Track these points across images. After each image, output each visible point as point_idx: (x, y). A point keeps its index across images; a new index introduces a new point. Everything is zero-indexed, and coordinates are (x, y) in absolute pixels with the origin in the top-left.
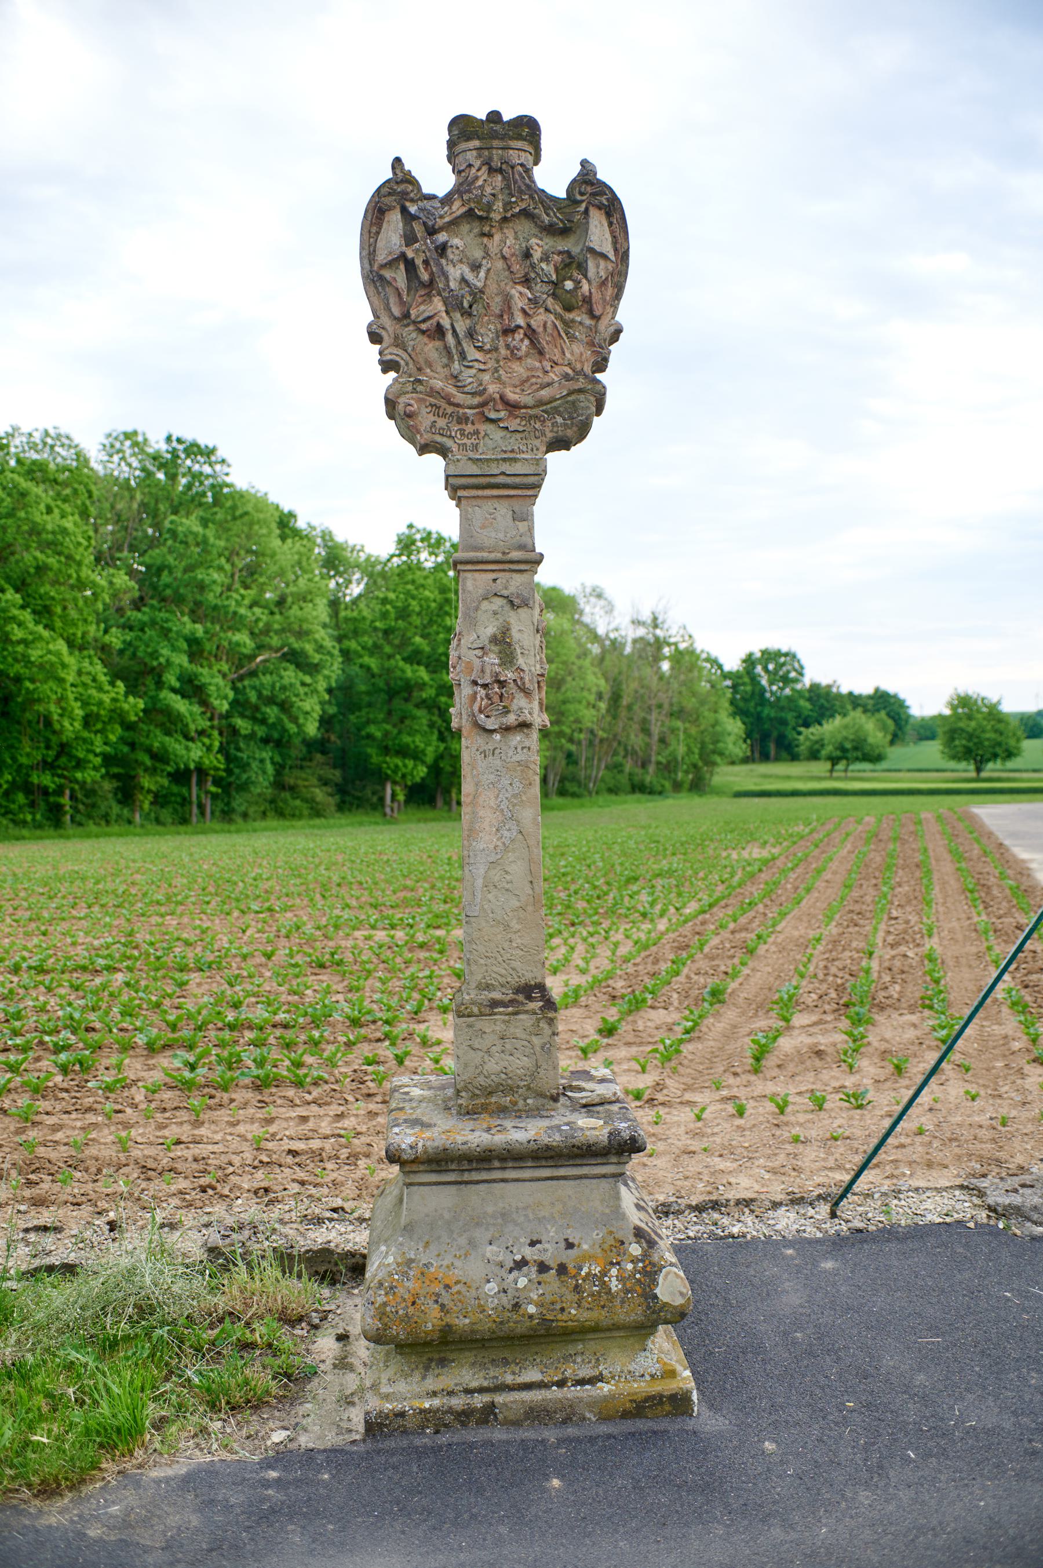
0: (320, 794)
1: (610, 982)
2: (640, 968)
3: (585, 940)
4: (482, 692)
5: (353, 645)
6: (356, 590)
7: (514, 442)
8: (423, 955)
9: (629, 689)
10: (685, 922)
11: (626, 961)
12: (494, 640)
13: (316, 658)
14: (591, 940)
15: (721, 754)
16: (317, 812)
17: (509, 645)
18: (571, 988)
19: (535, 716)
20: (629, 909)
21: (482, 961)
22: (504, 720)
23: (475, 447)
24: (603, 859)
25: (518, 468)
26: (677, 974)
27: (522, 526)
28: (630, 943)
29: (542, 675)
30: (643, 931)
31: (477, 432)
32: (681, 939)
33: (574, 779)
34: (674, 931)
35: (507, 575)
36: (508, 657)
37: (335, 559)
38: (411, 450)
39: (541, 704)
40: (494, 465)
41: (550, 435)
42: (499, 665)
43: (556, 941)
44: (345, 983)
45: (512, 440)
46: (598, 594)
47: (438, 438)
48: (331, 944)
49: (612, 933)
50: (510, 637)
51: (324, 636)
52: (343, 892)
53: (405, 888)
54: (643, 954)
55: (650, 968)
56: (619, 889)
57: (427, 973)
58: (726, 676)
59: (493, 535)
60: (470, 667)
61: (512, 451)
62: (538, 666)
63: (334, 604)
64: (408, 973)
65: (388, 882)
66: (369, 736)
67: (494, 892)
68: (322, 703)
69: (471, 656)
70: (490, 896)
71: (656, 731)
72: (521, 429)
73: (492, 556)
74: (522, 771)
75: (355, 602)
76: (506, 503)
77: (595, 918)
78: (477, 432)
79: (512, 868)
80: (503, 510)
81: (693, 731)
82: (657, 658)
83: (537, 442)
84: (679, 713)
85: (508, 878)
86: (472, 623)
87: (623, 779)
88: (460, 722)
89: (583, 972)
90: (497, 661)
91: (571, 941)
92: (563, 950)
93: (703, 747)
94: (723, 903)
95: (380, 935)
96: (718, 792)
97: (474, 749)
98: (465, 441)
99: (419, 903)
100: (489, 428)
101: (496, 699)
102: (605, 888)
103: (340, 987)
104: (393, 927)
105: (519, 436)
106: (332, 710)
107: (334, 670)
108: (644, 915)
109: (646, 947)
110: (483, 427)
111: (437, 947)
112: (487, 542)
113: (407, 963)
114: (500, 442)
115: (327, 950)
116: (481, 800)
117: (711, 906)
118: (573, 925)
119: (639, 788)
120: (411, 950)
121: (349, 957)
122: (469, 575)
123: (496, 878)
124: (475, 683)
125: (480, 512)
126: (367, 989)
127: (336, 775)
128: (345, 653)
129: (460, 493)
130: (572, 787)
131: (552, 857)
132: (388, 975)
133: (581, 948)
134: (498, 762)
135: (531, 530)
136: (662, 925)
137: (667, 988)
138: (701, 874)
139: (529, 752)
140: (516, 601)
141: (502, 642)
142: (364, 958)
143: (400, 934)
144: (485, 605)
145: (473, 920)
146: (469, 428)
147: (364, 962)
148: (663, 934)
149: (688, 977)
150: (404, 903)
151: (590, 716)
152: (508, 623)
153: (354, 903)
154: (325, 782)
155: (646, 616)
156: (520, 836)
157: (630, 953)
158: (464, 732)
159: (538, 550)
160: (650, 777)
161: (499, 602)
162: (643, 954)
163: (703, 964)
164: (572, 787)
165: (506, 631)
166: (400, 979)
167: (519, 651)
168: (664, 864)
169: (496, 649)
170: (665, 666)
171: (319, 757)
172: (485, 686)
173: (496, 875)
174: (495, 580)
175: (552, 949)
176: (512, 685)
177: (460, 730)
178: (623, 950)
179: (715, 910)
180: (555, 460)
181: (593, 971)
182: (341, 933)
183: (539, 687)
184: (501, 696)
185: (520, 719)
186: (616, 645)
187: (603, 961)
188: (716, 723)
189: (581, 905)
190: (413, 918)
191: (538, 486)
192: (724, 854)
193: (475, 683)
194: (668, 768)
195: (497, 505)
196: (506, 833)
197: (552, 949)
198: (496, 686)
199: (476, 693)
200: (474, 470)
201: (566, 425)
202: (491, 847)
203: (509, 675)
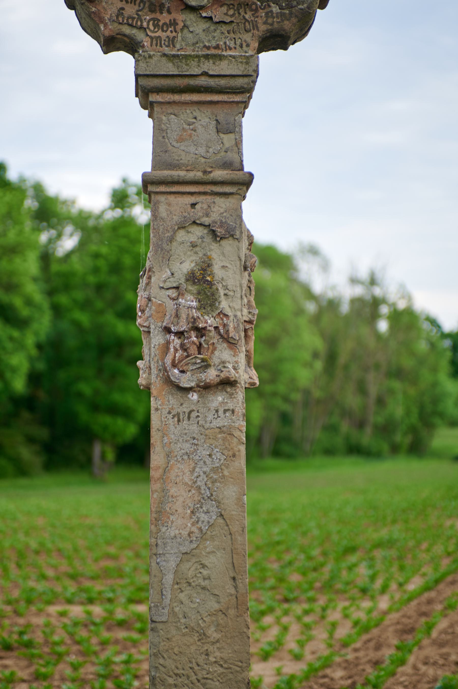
0: (26, 453)
1: (328, 671)
2: (361, 654)
3: (299, 619)
4: (177, 342)
5: (63, 299)
6: (69, 243)
7: (219, 37)
8: (122, 634)
9: (345, 349)
10: (410, 600)
11: (345, 645)
12: (192, 278)
13: (25, 312)
14: (307, 619)
15: (441, 415)
16: (22, 471)
17: (210, 284)
18: (285, 678)
19: (241, 371)
20: (347, 584)
21: (171, 681)
22: (203, 376)
23: (172, 42)
24: (319, 527)
25: (224, 68)
26: (403, 662)
27: (228, 139)
28: (349, 624)
29: (250, 322)
30: (362, 610)
31: (174, 23)
32: (405, 620)
33: (288, 439)
34: (398, 610)
35: (209, 199)
36: (208, 300)
37: (48, 212)
38: (94, 46)
39: (248, 357)
40: (194, 63)
41: (263, 28)
42: (198, 309)
43: (268, 620)
44: (32, 669)
45: (217, 34)
46: (313, 251)
47: (127, 30)
48: (21, 621)
49: (329, 612)
50: (212, 274)
51: (33, 290)
52: (41, 561)
53: (108, 557)
54: (365, 637)
55: (373, 655)
56: (337, 560)
57: (123, 657)
58: (445, 336)
59: (192, 149)
60: (161, 311)
61: (217, 47)
62: (245, 311)
63: (46, 258)
64: (103, 657)
65: (89, 549)
66: (80, 395)
67: (188, 591)
68: (31, 359)
69: (163, 297)
70: (182, 596)
71: (373, 390)
72: (228, 19)
73: (191, 175)
74: (224, 439)
75: (69, 255)
76: (208, 111)
77: (311, 594)
78: (174, 23)
79: (210, 561)
80: (204, 119)
81: (412, 391)
82: (375, 316)
83: (247, 37)
84: (398, 373)
85: (205, 572)
86: (166, 257)
87: (339, 441)
88: (149, 378)
89: (297, 658)
90: (194, 304)
91: (285, 620)
92: (275, 631)
93: (422, 408)
94: (450, 578)
95: (77, 611)
96: (438, 455)
97: (165, 412)
98: (159, 33)
99: (120, 574)
100: (190, 18)
101: (193, 350)
102: (321, 559)
103: (23, 674)
104: (91, 601)
105: (225, 28)
106: (41, 366)
107: (43, 325)
108: (364, 591)
109: (366, 630)
110: (182, 17)
111: (138, 625)
112: (185, 159)
113: (103, 644)
114: (202, 36)
115: (16, 629)
116: (172, 475)
117: (437, 582)
118: (286, 600)
119: (355, 450)
120: (109, 629)
121: (39, 637)
122: (162, 198)
123: (191, 573)
124: (167, 330)
125: (175, 122)
126: (57, 677)
127: (43, 433)
128: (57, 310)
129: (153, 98)
130: (286, 448)
131: (265, 523)
132: (81, 659)
133: (295, 628)
134: (195, 428)
135: (238, 144)
136: (384, 604)
137: (392, 680)
138: (424, 546)
139: (232, 413)
140: (220, 231)
141: (202, 282)
142: (56, 638)
143: (97, 610)
144: (181, 235)
145: (160, 626)
146: (165, 18)
147: (56, 644)
148: (385, 613)
149: (415, 667)
150: (105, 574)
151: (305, 375)
152: (210, 258)
153: (50, 573)
154: (31, 440)
155: (363, 274)
156: (221, 521)
157: (350, 636)
158: (154, 391)
159: (246, 169)
160: (366, 438)
161: (198, 231)
162: (365, 637)
163: (431, 652)
164: (286, 448)
165: (206, 266)
166: (93, 664)
167: (222, 292)
168: (384, 533)
169: (194, 289)
170: (383, 326)
171: (26, 415)
172: (180, 334)
173: (189, 569)
174: (193, 205)
175: (263, 629)
176: (213, 333)
177: (148, 388)
178: (342, 632)
179: (441, 586)
180: (268, 60)
181: (308, 657)
182: (33, 608)
183: (246, 336)
184: (200, 347)
185: (222, 375)
186: (332, 305)
187: (319, 644)
188: (435, 384)
189: (294, 578)
190: (113, 591)
191: (248, 91)
192: (449, 523)
193: (167, 330)
194: (386, 429)
195: (197, 113)
196: (203, 517)
197: (263, 629)
198: (193, 334)
199: (168, 343)
200: (170, 69)
201: (282, 15)
202: (185, 533)
203: (210, 321)
